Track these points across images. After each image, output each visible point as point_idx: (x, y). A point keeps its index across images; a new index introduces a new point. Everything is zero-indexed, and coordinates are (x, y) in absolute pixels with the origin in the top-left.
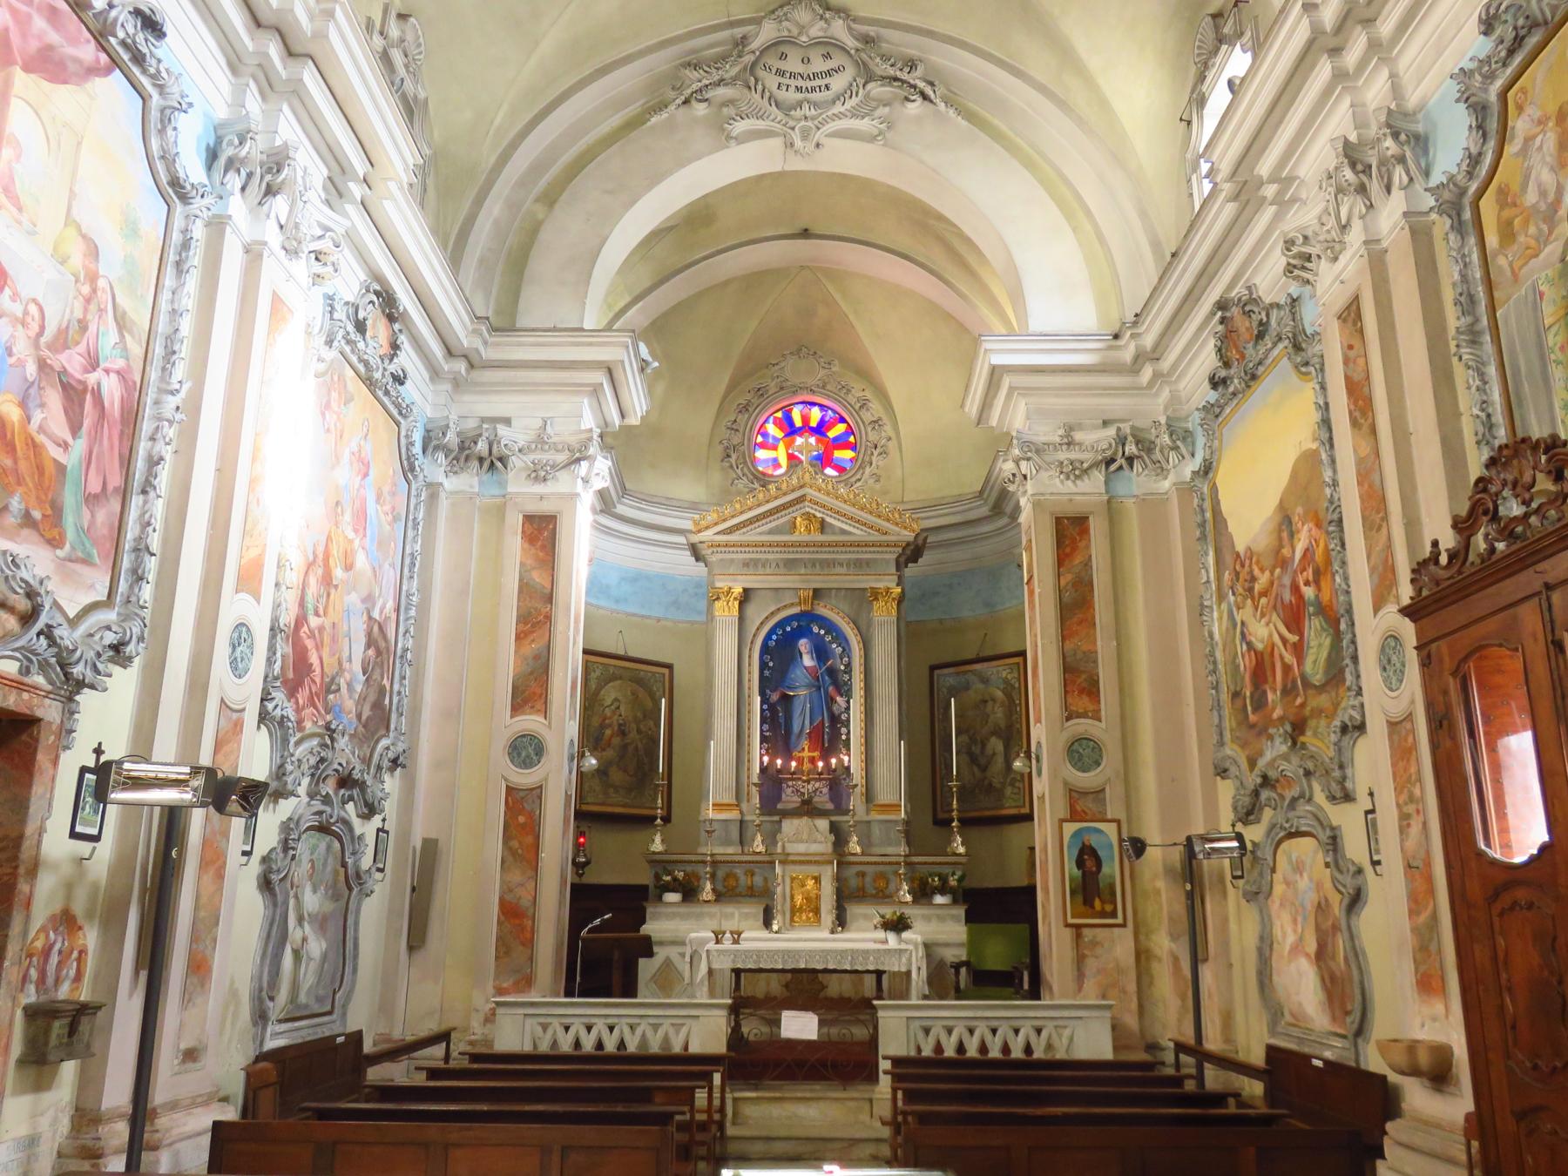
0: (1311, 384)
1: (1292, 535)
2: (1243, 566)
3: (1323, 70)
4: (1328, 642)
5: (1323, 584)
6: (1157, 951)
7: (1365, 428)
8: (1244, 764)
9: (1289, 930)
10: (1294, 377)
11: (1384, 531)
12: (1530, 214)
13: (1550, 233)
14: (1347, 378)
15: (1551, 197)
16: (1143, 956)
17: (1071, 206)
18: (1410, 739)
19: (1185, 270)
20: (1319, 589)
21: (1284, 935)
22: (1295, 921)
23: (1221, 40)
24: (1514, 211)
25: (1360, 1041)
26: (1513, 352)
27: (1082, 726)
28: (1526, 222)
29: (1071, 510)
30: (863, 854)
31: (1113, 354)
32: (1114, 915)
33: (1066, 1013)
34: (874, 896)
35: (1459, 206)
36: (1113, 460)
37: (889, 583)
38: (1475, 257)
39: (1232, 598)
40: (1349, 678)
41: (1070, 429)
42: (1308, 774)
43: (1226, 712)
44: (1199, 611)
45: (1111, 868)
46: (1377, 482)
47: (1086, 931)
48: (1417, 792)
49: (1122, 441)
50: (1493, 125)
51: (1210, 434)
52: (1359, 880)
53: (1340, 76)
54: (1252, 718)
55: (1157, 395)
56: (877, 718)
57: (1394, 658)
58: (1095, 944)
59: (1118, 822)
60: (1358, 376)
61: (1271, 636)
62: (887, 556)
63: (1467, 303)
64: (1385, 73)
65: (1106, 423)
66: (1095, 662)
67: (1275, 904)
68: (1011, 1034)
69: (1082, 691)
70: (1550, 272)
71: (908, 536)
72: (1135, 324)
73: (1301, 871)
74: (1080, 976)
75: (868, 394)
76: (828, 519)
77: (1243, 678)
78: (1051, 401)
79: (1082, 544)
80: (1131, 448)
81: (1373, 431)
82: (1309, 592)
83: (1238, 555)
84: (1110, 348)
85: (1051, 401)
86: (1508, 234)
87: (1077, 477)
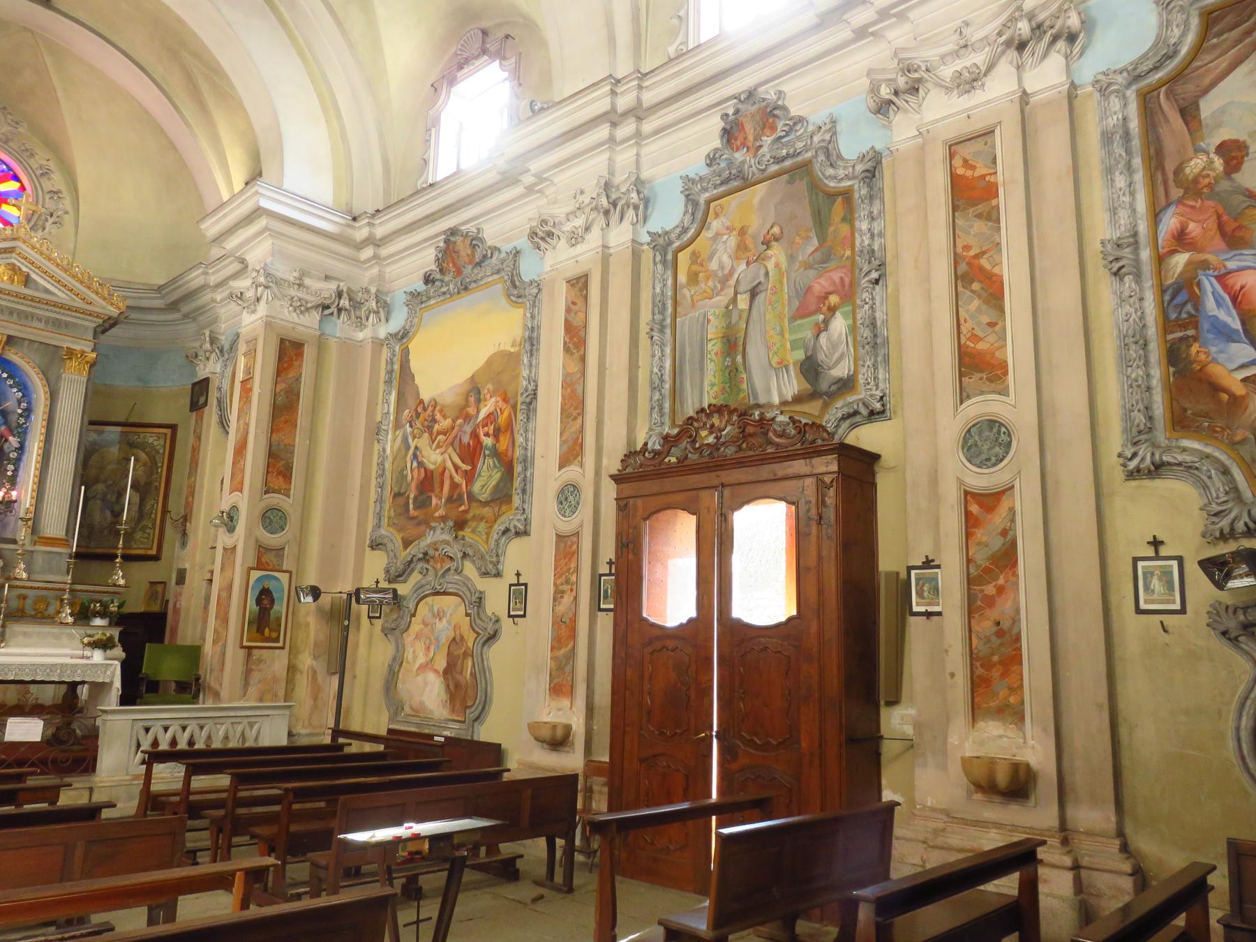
0: (521, 311)
1: (478, 401)
2: (425, 409)
3: (603, 132)
4: (498, 476)
5: (501, 439)
6: (301, 667)
7: (577, 355)
8: (399, 543)
9: (421, 654)
10: (503, 301)
11: (579, 421)
12: (710, 275)
13: (722, 290)
14: (566, 321)
15: (726, 272)
16: (292, 669)
17: (330, 106)
18: (575, 547)
19: (434, 198)
20: (498, 441)
21: (415, 657)
22: (428, 649)
23: (484, 51)
24: (700, 268)
25: (476, 724)
26: (683, 346)
27: (275, 499)
28: (708, 278)
29: (293, 336)
30: (29, 580)
31: (349, 231)
32: (277, 640)
33: (258, 713)
34: (33, 617)
35: (664, 247)
36: (328, 307)
37: (84, 346)
38: (670, 282)
39: (409, 429)
40: (516, 501)
41: (303, 274)
42: (465, 555)
43: (387, 506)
44: (376, 431)
45: (280, 608)
46: (579, 389)
47: (255, 652)
48: (574, 578)
49: (340, 295)
50: (699, 215)
51: (412, 313)
52: (497, 626)
53: (612, 140)
54: (412, 512)
55: (367, 269)
56: (53, 462)
57: (571, 498)
58: (260, 661)
59: (290, 573)
60: (577, 321)
61: (444, 461)
62: (86, 323)
63: (659, 306)
64: (634, 151)
65: (327, 278)
66: (292, 453)
67: (409, 638)
68: (161, 731)
69: (279, 473)
70: (717, 311)
71: (113, 311)
72: (373, 216)
73: (443, 617)
74: (246, 684)
75: (52, 165)
76: (33, 276)
77: (409, 485)
78: (292, 249)
79: (296, 364)
80: (344, 302)
81: (583, 359)
82: (488, 441)
83: (422, 402)
84: (348, 226)
85: (292, 249)
86: (693, 278)
87: (302, 312)
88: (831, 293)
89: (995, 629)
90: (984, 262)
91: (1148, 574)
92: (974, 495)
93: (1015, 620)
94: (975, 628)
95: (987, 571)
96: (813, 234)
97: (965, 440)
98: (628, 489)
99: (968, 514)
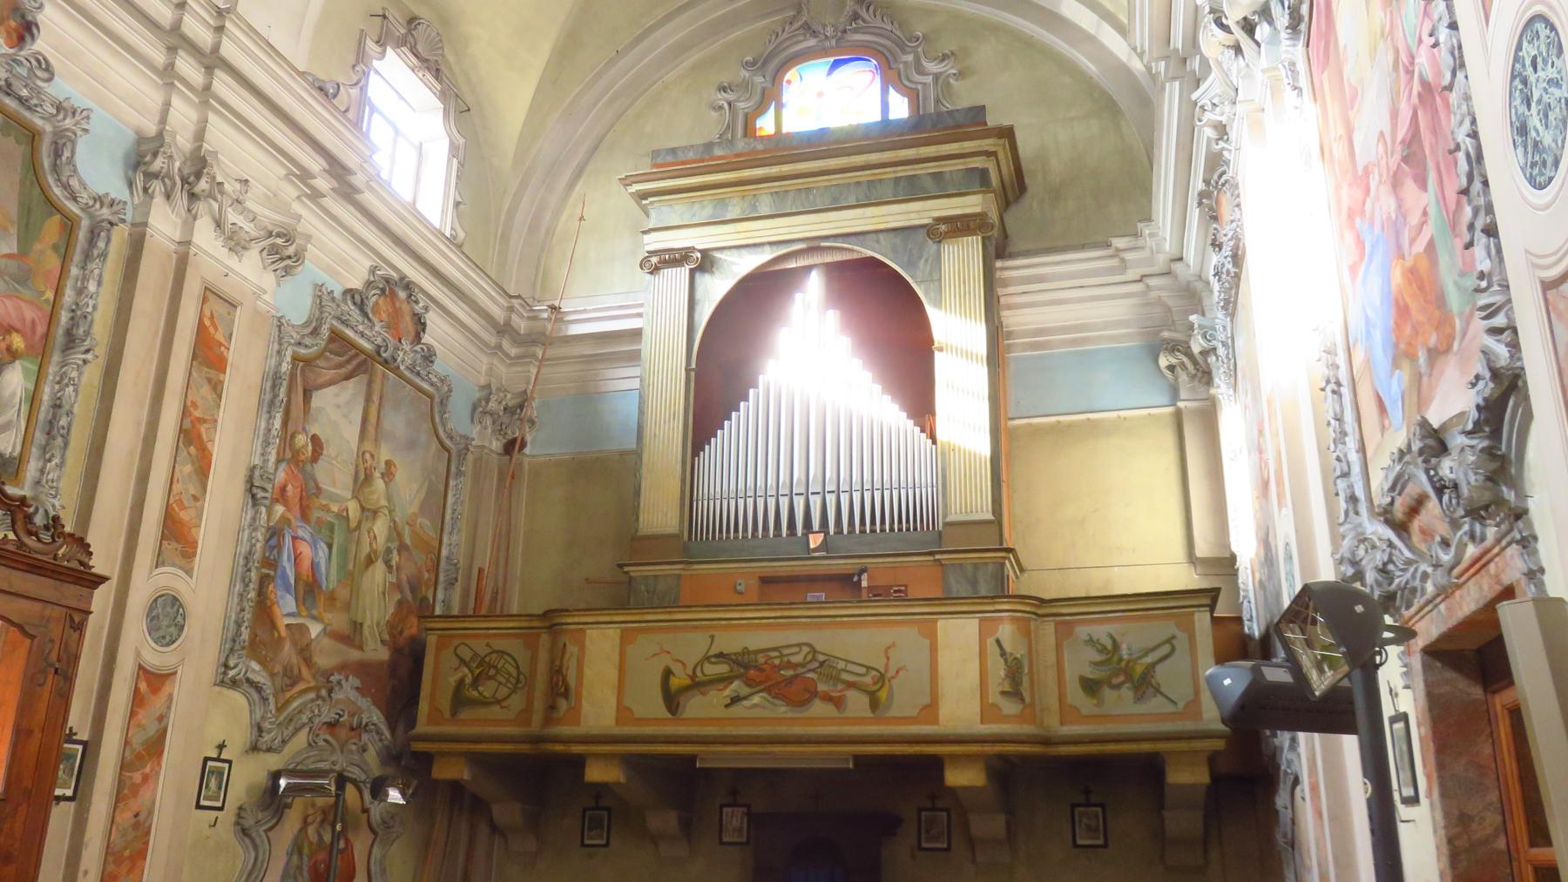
88: (17, 331)
89: (133, 821)
90: (203, 429)
91: (212, 772)
92: (146, 671)
93: (150, 813)
94: (118, 819)
95: (139, 757)
96: (13, 231)
97: (151, 609)
98: (82, 606)
99: (137, 690)
